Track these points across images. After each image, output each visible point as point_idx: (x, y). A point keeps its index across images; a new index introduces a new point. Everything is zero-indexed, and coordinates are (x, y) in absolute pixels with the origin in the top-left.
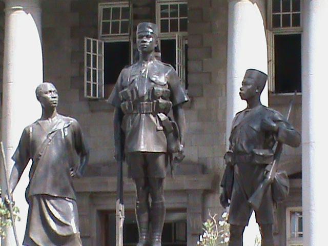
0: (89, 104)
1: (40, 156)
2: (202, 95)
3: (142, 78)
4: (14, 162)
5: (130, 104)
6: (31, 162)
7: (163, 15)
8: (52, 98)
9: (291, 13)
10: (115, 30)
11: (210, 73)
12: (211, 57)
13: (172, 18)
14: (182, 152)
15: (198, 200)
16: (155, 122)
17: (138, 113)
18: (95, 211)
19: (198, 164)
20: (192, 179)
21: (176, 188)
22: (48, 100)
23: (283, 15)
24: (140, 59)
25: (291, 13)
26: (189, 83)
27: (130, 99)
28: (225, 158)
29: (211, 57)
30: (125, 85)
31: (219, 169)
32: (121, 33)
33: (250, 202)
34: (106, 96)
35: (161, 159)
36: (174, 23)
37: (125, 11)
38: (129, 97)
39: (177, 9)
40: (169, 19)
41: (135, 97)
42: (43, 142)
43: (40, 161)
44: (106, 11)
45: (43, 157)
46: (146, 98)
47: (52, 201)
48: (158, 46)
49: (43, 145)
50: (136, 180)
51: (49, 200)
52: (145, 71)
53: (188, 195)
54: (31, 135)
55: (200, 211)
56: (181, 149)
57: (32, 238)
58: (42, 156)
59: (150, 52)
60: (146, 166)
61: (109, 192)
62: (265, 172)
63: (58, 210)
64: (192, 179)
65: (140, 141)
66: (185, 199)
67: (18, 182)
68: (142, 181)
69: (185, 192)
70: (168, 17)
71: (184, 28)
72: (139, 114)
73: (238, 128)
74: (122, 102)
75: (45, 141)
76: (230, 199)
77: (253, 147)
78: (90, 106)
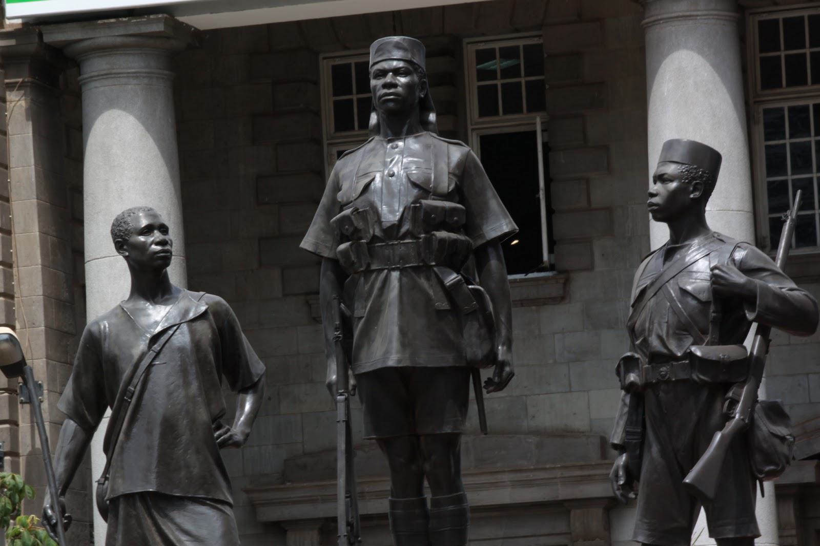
6: (109, 412)
7: (483, 75)
14: (503, 364)
23: (791, 144)
26: (657, 294)
28: (618, 373)
34: (386, 269)
36: (512, 93)
39: (518, 57)
40: (499, 82)
48: (426, 95)
51: (166, 516)
56: (500, 357)
62: (727, 403)
65: (712, 452)
70: (496, 79)
71: (537, 103)
73: (650, 293)
76: (112, 408)
77: (691, 340)
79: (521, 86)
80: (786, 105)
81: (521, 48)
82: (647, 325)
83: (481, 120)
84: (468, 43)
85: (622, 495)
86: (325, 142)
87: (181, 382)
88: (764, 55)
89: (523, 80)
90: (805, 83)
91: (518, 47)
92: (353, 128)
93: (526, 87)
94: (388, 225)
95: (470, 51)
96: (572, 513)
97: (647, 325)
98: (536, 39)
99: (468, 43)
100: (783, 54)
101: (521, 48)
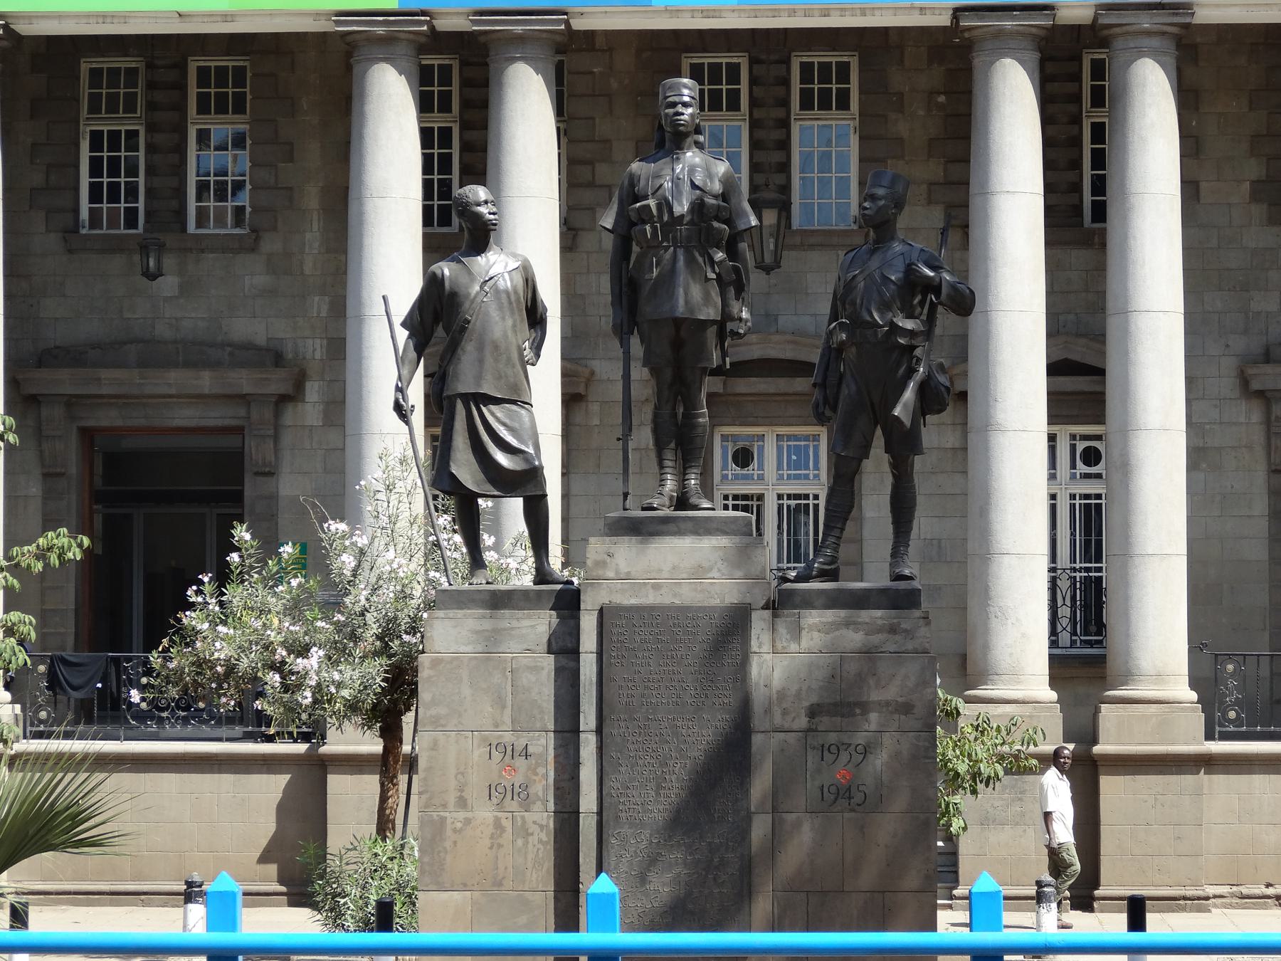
0: (64, 238)
1: (469, 322)
2: (274, 229)
3: (676, 181)
4: (407, 333)
5: (654, 229)
8: (490, 213)
9: (436, 89)
10: (112, 108)
11: (291, 189)
12: (291, 160)
13: (235, 90)
15: (268, 413)
16: (703, 265)
17: (670, 246)
18: (75, 430)
19: (268, 350)
20: (259, 376)
21: (228, 391)
22: (484, 217)
24: (667, 144)
25: (230, 91)
27: (655, 219)
29: (291, 160)
30: (643, 193)
31: (304, 358)
32: (124, 113)
33: (896, 414)
35: (711, 333)
37: (132, 72)
38: (653, 216)
41: (666, 218)
42: (473, 295)
43: (468, 331)
44: (95, 74)
45: (475, 324)
46: (687, 219)
47: (492, 407)
49: (473, 302)
50: (655, 372)
52: (683, 169)
53: (39, 402)
54: (447, 284)
55: (271, 432)
57: (453, 471)
58: (471, 324)
59: (686, 135)
60: (677, 345)
61: (101, 396)
63: (504, 424)
64: (259, 376)
66: (242, 412)
67: (417, 368)
68: (668, 374)
69: (244, 399)
72: (672, 248)
74: (635, 224)
75: (477, 293)
78: (66, 241)
79: (102, 96)
80: (436, 126)
81: (230, 68)
82: (1061, 346)
83: (198, 116)
84: (192, 61)
85: (354, 544)
86: (82, 123)
87: (521, 455)
88: (802, 86)
89: (230, 91)
90: (227, 113)
91: (103, 68)
92: (210, 113)
93: (232, 96)
94: (678, 214)
95: (193, 66)
96: (553, 613)
97: (1061, 346)
98: (242, 62)
99: (192, 61)
100: (724, 87)
101: (230, 68)
